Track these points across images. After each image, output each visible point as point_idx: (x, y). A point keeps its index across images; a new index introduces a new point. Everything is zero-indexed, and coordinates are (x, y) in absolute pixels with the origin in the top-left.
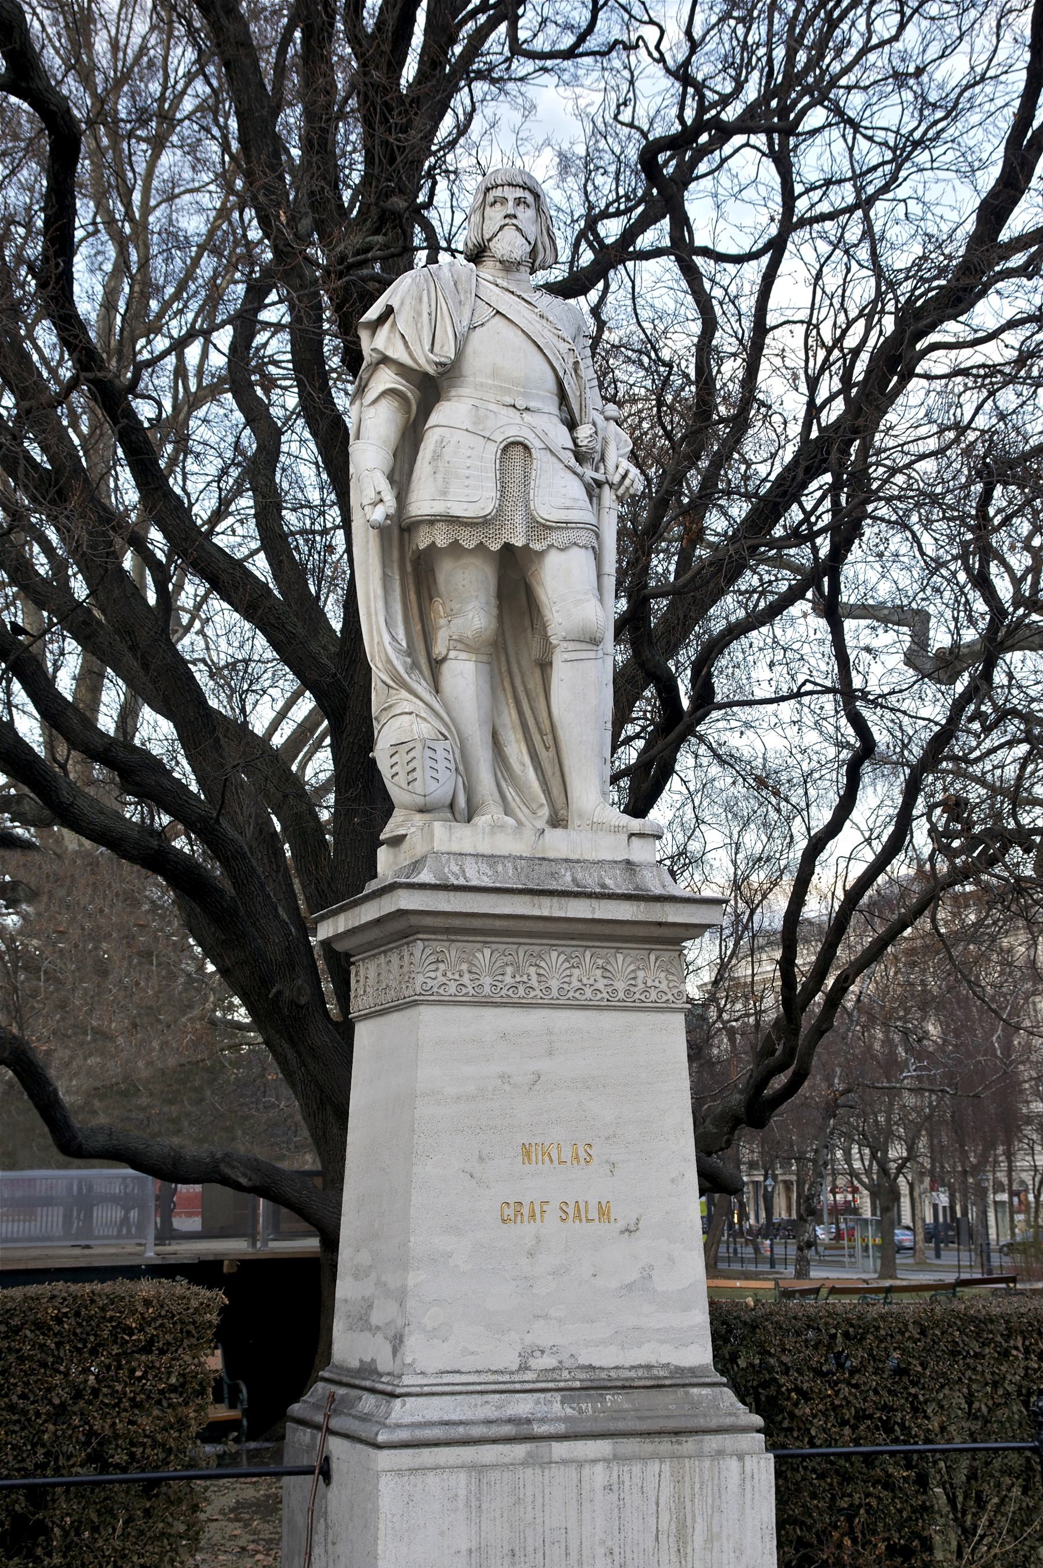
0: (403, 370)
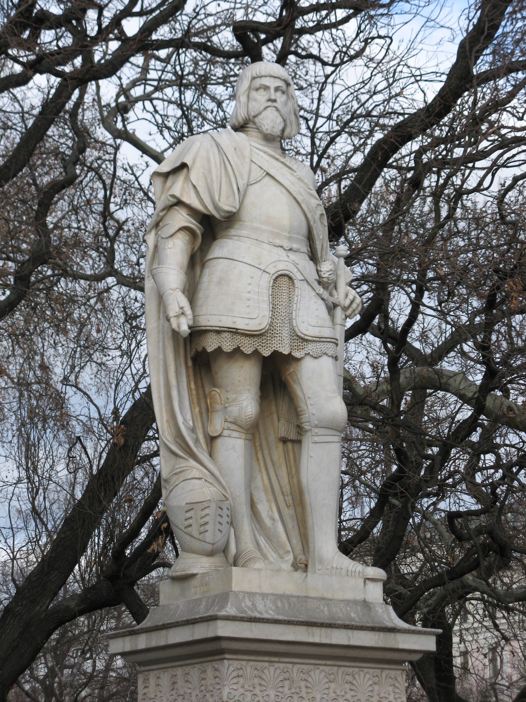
0: (193, 211)
